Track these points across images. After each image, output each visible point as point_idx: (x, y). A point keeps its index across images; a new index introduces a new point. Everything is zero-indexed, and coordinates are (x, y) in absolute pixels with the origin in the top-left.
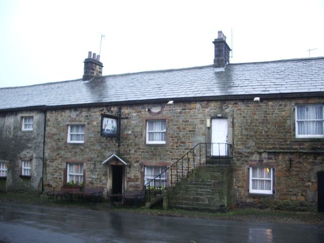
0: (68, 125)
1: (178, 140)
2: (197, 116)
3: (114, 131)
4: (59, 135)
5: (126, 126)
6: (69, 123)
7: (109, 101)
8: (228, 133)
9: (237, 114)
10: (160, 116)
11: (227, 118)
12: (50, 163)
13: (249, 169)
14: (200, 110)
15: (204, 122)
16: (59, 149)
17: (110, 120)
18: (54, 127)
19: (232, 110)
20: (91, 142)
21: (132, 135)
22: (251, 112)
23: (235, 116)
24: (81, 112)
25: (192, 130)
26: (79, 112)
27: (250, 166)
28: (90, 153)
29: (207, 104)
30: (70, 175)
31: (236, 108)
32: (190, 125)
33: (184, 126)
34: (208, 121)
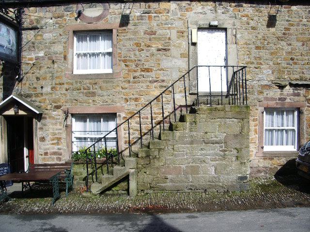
10: (101, 25)
14: (177, 15)
31: (240, 13)
32: (159, 39)
33: (148, 42)
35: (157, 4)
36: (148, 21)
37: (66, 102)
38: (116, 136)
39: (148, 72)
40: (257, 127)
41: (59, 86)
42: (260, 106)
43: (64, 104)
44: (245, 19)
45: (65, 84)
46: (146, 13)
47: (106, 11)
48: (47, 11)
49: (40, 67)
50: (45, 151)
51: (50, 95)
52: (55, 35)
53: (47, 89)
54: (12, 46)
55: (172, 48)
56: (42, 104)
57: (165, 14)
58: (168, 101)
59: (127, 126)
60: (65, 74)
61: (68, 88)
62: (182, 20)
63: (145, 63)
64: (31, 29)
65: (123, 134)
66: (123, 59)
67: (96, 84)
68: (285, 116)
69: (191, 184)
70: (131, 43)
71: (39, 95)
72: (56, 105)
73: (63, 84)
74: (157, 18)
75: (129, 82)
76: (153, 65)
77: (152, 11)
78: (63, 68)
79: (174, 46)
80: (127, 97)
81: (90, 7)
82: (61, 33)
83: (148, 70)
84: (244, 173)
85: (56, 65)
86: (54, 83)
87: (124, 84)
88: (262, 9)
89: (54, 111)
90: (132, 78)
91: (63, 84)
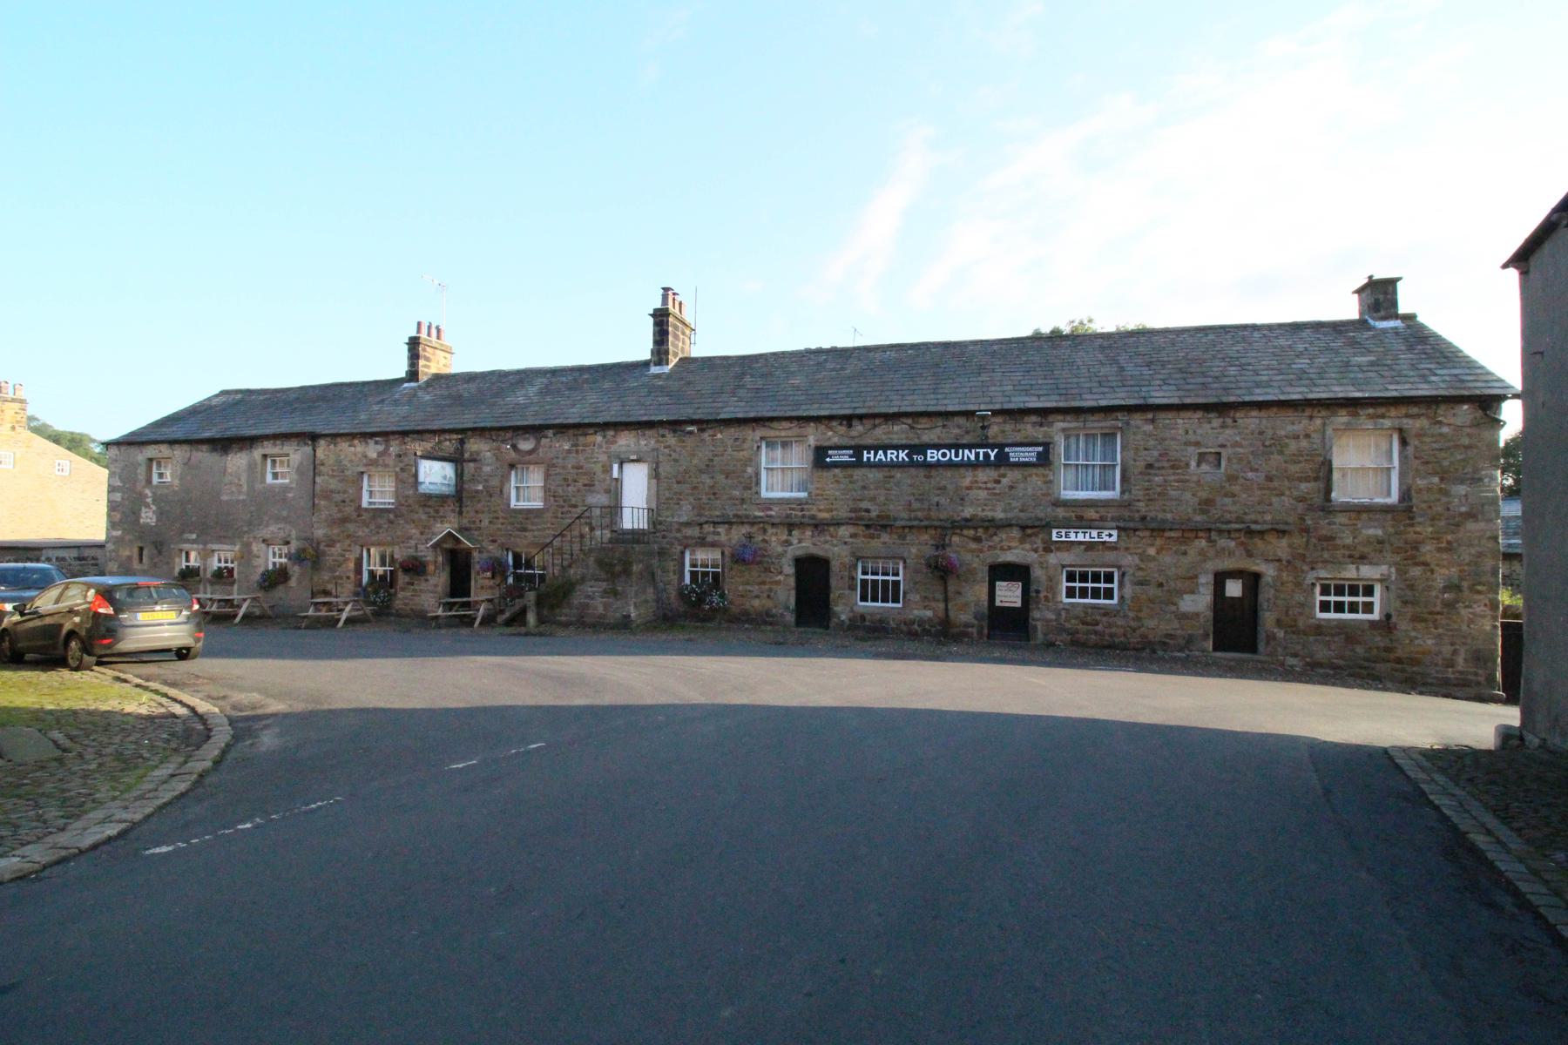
12: (326, 549)
18: (333, 476)
32: (585, 474)
44: (667, 451)
64: (470, 461)
83: (575, 506)
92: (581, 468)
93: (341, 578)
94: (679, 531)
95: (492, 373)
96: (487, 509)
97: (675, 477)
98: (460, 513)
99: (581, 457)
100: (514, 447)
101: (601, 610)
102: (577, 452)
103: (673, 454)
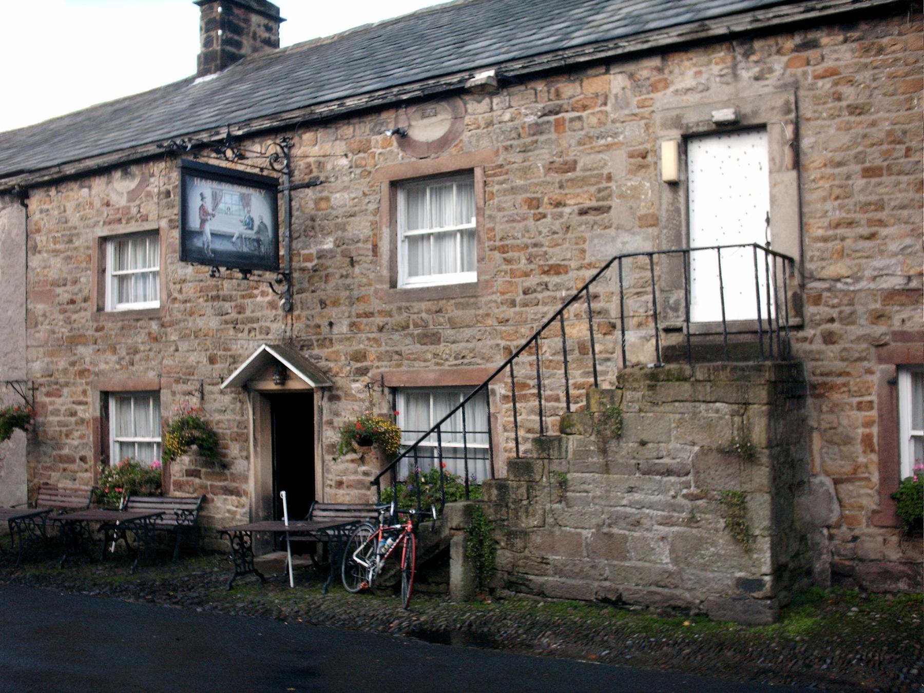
0: (104, 240)
1: (529, 260)
2: (616, 135)
3: (258, 241)
4: (75, 282)
5: (313, 219)
6: (105, 232)
7: (399, 208)
8: (773, 200)
9: (819, 101)
10: (448, 161)
11: (761, 128)
12: (47, 400)
13: (893, 383)
14: (627, 105)
15: (650, 158)
16: (75, 340)
17: (231, 195)
18: (56, 252)
19: (788, 79)
20: (185, 301)
21: (339, 257)
22: (891, 77)
23: (807, 109)
24: (144, 182)
25: (594, 203)
26: (137, 181)
27: (900, 368)
28: (183, 346)
29: (660, 70)
30: (122, 444)
31: (810, 69)
32: (584, 181)
33: (556, 194)
34: (668, 152)
35: (577, 84)
36: (553, 136)
37: (379, 359)
38: (487, 446)
39: (558, 273)
40: (875, 430)
41: (364, 320)
42: (881, 360)
43: (376, 364)
44: (825, 85)
45: (376, 315)
46: (551, 113)
47: (458, 122)
48: (336, 139)
49: (327, 276)
50: (338, 478)
51: (347, 343)
52: (353, 195)
53: (342, 328)
54: (258, 232)
55: (615, 202)
56: (331, 365)
57: (597, 109)
58: (607, 352)
59: (512, 419)
60: (376, 291)
61: (381, 324)
62: (642, 118)
63: (550, 251)
64: (307, 186)
65: (505, 442)
66: (498, 243)
67: (440, 311)
68: (764, 408)
69: (607, 584)
70: (520, 198)
71: (327, 343)
72: (359, 365)
73: (371, 314)
74: (577, 125)
75: (513, 304)
76: (569, 255)
77: (565, 106)
78: (372, 276)
79: (621, 196)
80: (508, 343)
81: (424, 117)
82: (366, 190)
83: (557, 270)
84: (754, 570)
85: (357, 270)
86: (354, 314)
87: (501, 309)
88: (885, 41)
89: (354, 381)
90: (521, 292)
91: (371, 314)
92: (571, 166)
93: (71, 460)
94: (878, 317)
95: (355, 33)
96: (344, 294)
97: (859, 158)
98: (290, 309)
99: (569, 139)
100: (401, 135)
101: (664, 559)
102: (559, 125)
103: (848, 91)
